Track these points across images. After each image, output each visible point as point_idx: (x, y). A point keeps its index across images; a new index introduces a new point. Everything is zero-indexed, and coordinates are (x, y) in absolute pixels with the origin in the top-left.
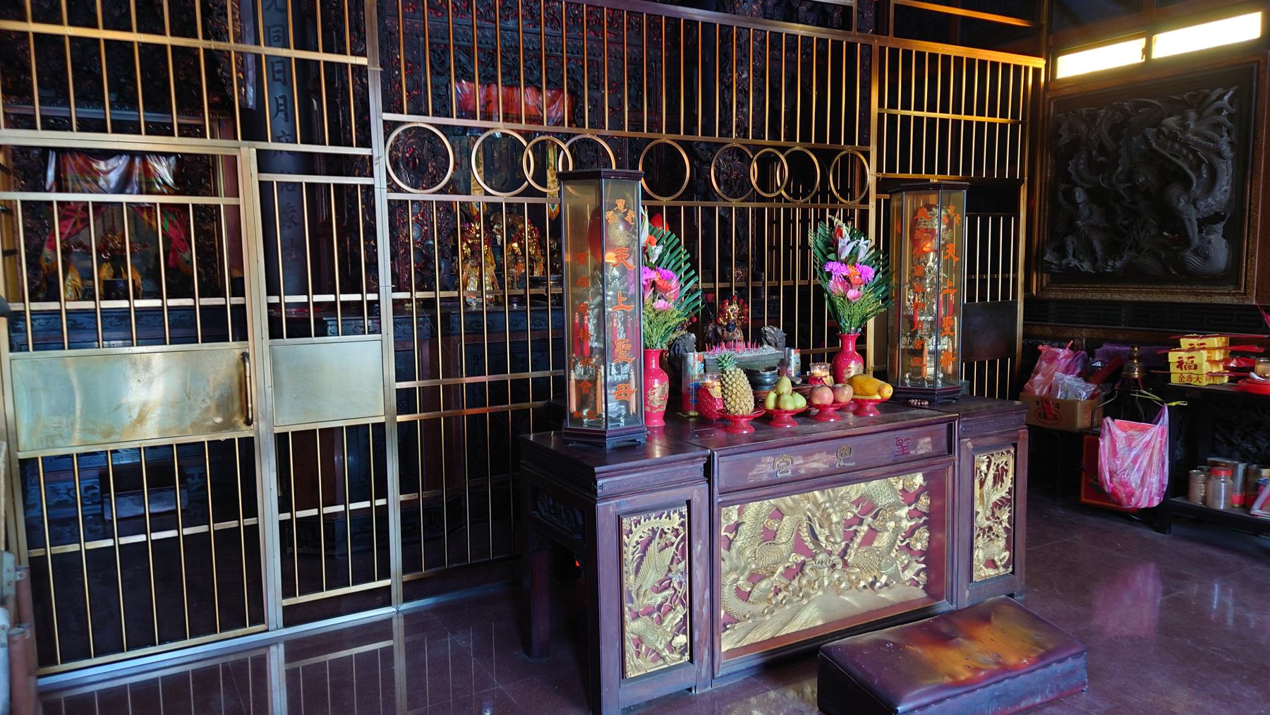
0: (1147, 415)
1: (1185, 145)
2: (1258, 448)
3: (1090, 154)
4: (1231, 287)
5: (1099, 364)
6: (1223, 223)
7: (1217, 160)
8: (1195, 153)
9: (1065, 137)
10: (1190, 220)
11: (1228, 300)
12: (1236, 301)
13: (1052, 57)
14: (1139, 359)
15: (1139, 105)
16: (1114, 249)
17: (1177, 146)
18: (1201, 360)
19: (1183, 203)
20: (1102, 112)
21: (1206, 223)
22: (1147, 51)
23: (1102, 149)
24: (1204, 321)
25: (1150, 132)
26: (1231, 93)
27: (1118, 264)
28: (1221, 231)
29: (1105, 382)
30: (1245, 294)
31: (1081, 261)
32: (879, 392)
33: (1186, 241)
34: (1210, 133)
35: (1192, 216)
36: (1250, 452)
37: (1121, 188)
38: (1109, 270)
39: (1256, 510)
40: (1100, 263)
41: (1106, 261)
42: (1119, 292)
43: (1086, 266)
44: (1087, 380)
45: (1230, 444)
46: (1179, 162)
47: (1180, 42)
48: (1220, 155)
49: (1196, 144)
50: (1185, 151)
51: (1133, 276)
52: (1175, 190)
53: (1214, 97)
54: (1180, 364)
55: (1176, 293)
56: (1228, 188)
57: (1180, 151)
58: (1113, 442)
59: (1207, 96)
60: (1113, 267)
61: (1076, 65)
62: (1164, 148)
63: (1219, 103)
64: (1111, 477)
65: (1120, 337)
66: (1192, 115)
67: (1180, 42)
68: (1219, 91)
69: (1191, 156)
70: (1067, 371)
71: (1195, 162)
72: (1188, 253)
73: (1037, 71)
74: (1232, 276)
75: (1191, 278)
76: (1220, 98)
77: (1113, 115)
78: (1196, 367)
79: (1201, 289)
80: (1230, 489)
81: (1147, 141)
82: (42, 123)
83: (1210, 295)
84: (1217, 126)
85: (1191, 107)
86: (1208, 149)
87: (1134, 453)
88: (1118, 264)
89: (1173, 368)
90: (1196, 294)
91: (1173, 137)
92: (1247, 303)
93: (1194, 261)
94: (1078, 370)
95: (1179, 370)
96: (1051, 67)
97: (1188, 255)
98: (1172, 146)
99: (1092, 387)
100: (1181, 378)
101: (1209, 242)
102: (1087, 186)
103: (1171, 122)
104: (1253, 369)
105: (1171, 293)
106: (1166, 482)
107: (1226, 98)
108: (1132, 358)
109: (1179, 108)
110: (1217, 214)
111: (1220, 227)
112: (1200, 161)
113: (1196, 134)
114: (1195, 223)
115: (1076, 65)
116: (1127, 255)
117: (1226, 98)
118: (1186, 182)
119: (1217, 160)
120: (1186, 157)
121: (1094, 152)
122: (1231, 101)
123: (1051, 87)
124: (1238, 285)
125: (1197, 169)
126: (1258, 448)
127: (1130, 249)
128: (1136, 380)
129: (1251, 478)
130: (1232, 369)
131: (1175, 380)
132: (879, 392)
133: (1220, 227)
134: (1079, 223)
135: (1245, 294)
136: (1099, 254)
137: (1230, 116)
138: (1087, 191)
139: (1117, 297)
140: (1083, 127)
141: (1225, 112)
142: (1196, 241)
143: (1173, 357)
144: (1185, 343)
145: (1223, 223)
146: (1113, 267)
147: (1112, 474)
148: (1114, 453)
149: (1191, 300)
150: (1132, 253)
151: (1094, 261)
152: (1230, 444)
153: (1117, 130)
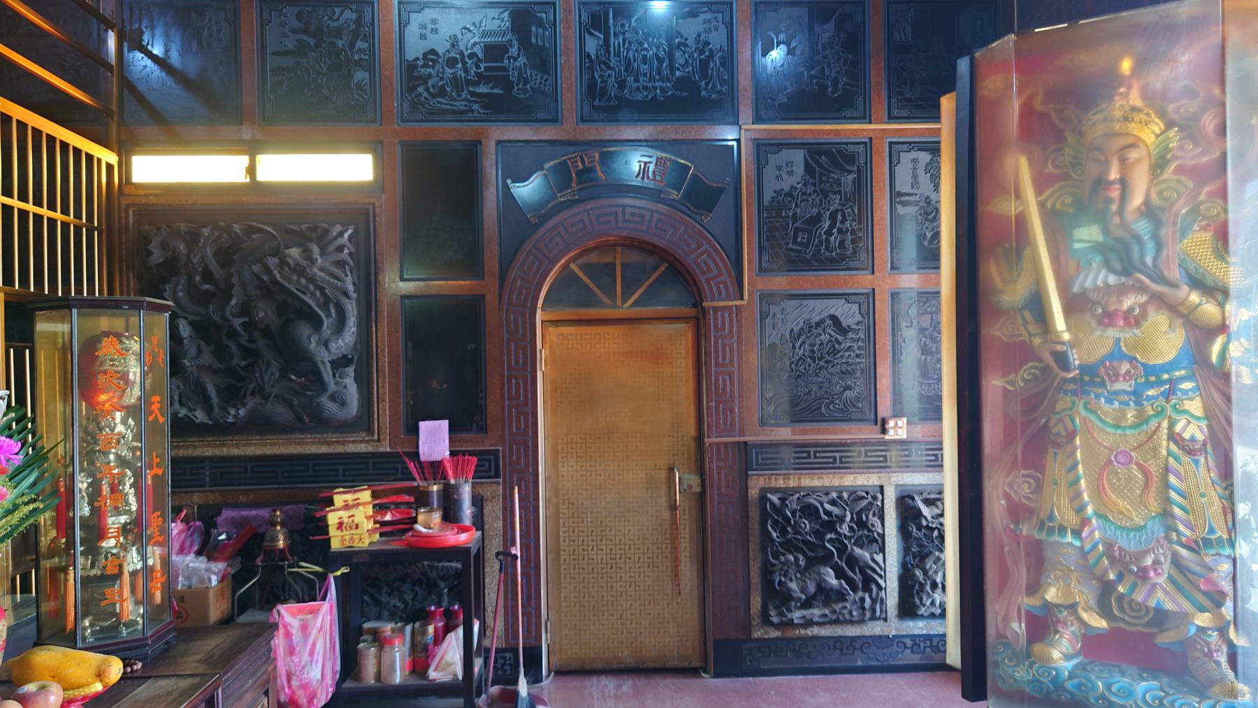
0: (310, 592)
1: (312, 280)
2: (405, 602)
3: (190, 279)
4: (364, 434)
5: (223, 537)
6: (353, 367)
7: (345, 301)
8: (322, 290)
9: (157, 257)
10: (323, 362)
11: (362, 448)
12: (370, 449)
13: (125, 149)
14: (283, 524)
15: (250, 230)
16: (232, 394)
17: (303, 281)
18: (353, 519)
19: (314, 344)
20: (206, 231)
21: (340, 364)
22: (251, 170)
23: (207, 275)
24: (352, 471)
25: (272, 262)
26: (350, 232)
27: (242, 412)
28: (352, 374)
29: (233, 556)
30: (379, 440)
31: (190, 410)
32: (100, 675)
33: (322, 386)
34: (336, 271)
35: (324, 358)
36: (397, 608)
37: (237, 323)
38: (231, 420)
39: (432, 674)
40: (216, 411)
41: (224, 409)
42: (238, 446)
43: (200, 416)
44: (210, 558)
45: (377, 602)
46: (306, 298)
47: (287, 168)
48: (346, 294)
49: (323, 281)
50: (312, 288)
51: (260, 425)
52: (303, 330)
53: (335, 233)
54: (340, 526)
55: (306, 444)
56: (354, 329)
57: (306, 287)
58: (288, 635)
59: (326, 232)
60: (235, 416)
61: (154, 169)
62: (290, 282)
63: (340, 241)
64: (289, 680)
65: (242, 498)
66: (316, 250)
67: (287, 168)
68: (338, 228)
69: (318, 293)
70: (181, 551)
71: (322, 299)
72: (324, 399)
73: (110, 167)
74: (364, 422)
75: (320, 423)
76: (341, 234)
77: (220, 236)
78: (357, 527)
79: (334, 437)
80: (402, 657)
81: (268, 270)
82: (444, 469)
83: (343, 443)
84: (341, 264)
85: (311, 240)
86: (336, 287)
87: (310, 641)
88: (242, 412)
89: (333, 531)
90: (328, 443)
91: (300, 270)
92: (381, 450)
93: (330, 407)
94: (196, 548)
95: (339, 533)
96: (125, 165)
97: (324, 399)
98: (298, 281)
99: (220, 566)
100: (343, 540)
101: (345, 387)
102: (191, 317)
103: (294, 252)
104: (415, 521)
105: (300, 443)
106: (338, 668)
107: (346, 236)
108: (274, 524)
109: (301, 239)
110: (344, 356)
111: (351, 370)
112: (327, 299)
113: (322, 270)
114: (329, 365)
115: (154, 169)
116: (251, 402)
117: (346, 236)
118: (316, 323)
119: (345, 301)
120: (313, 294)
121: (198, 278)
122: (350, 238)
123: (126, 190)
124: (369, 430)
125: (325, 307)
126: (405, 602)
127: (253, 394)
128: (282, 551)
129: (418, 638)
130: (383, 524)
131: (335, 545)
132: (100, 675)
133: (351, 370)
134: (186, 362)
135: (379, 440)
136: (215, 400)
137: (350, 254)
138: (191, 323)
139: (235, 452)
140: (182, 246)
141: (346, 251)
142: (332, 387)
143: (332, 519)
144: (339, 500)
145: (353, 367)
146: (235, 416)
147: (289, 677)
148: (291, 651)
149: (324, 450)
150: (257, 400)
151: (209, 410)
152: (377, 602)
153: (226, 255)
